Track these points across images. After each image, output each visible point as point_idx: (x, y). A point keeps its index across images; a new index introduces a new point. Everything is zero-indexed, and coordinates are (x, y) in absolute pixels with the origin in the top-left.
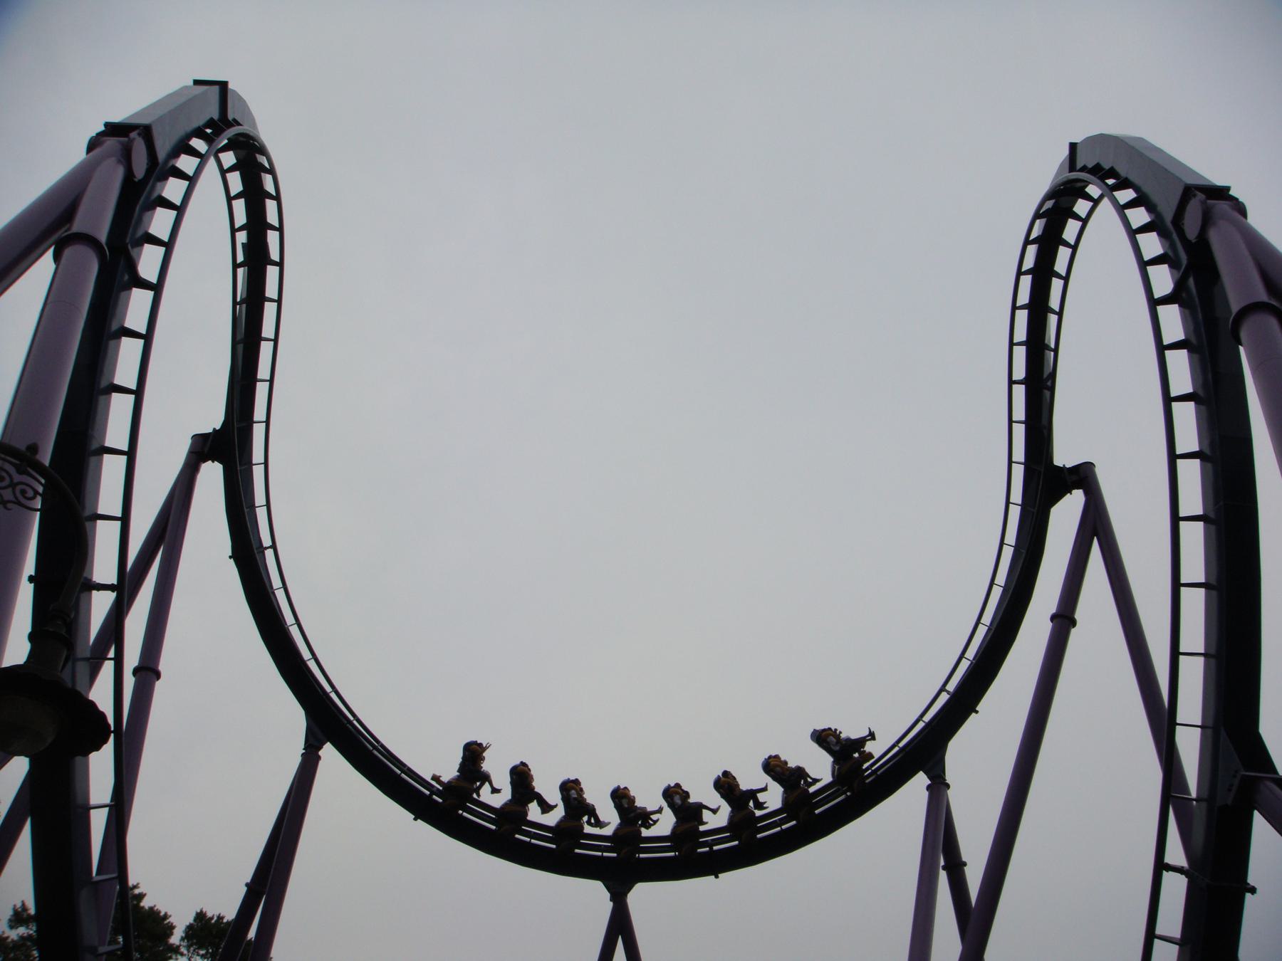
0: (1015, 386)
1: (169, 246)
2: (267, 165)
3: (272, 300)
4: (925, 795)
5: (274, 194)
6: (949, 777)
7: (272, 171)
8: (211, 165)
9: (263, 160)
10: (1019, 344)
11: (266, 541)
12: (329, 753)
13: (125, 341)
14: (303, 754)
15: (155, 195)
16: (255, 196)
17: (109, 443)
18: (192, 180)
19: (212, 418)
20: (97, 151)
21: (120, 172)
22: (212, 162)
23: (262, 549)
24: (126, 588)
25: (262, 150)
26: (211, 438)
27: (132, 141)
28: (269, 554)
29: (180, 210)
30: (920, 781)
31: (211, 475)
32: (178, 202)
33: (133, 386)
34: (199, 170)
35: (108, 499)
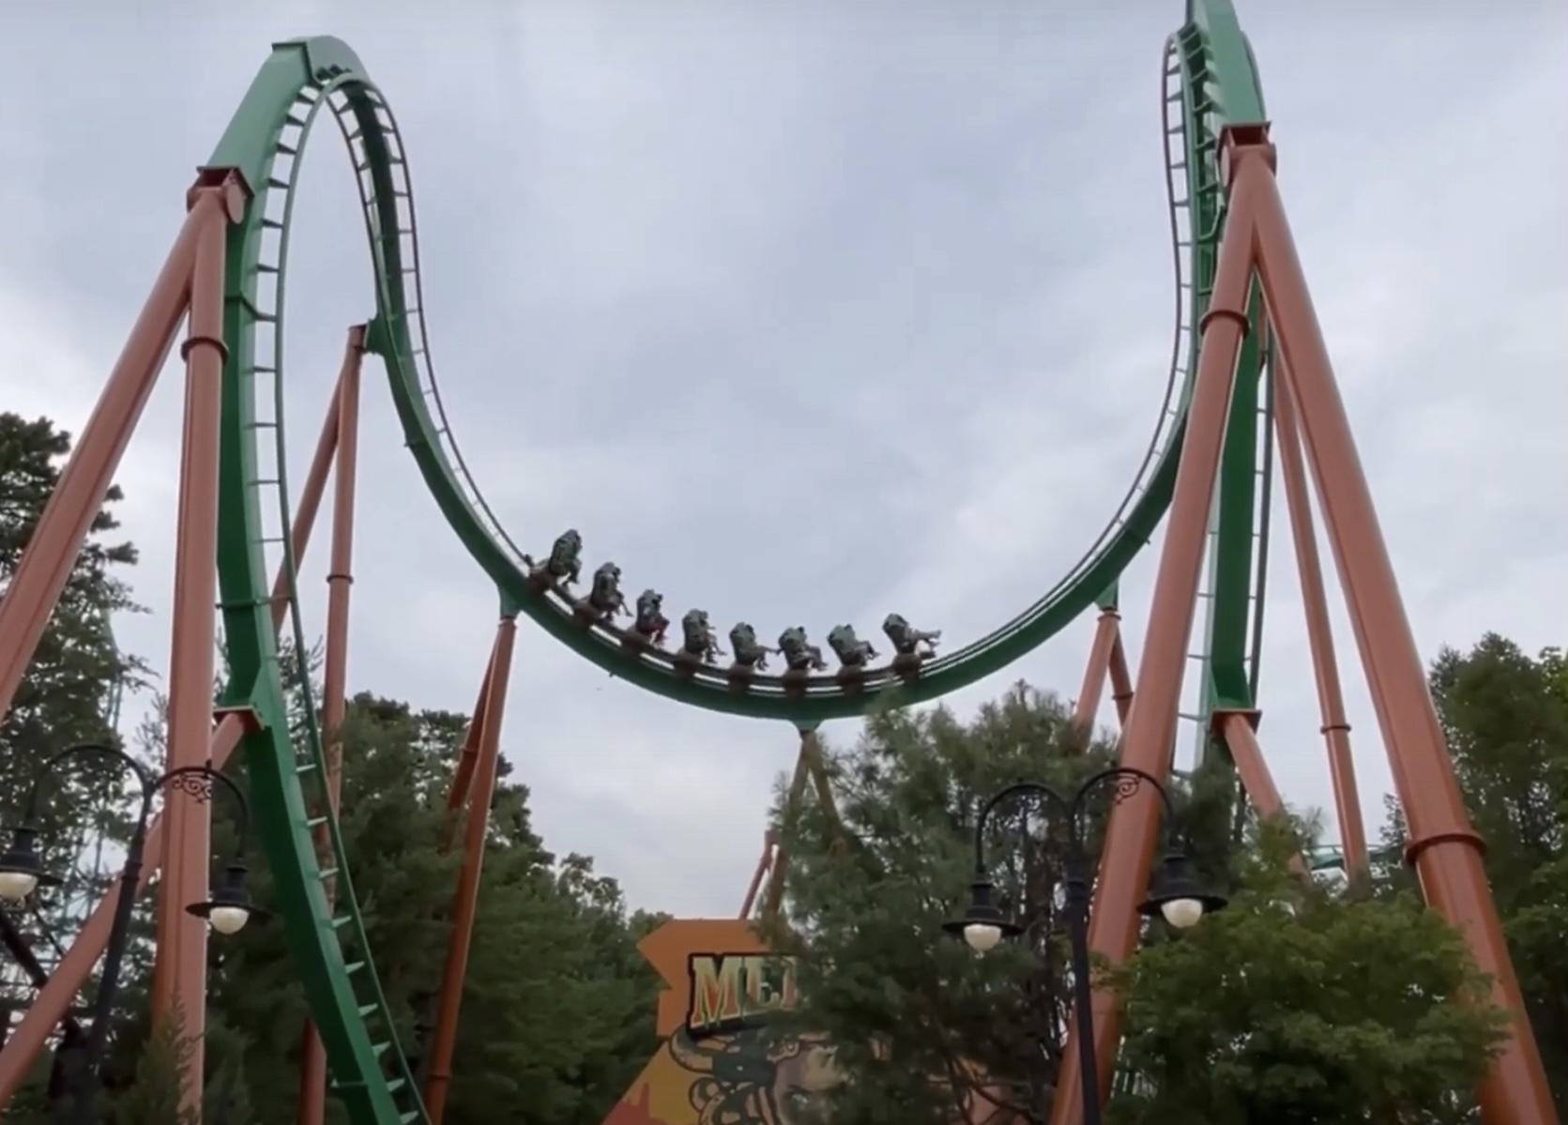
0: (1178, 210)
1: (289, 187)
2: (378, 100)
3: (405, 231)
4: (1096, 625)
5: (391, 127)
6: (1121, 611)
7: (384, 105)
8: (324, 109)
9: (370, 94)
10: (1177, 166)
11: (438, 425)
12: (524, 621)
13: (261, 276)
14: (500, 626)
15: (265, 177)
16: (373, 136)
17: (259, 419)
18: (305, 125)
19: (366, 310)
20: (198, 205)
21: (223, 223)
22: (324, 107)
23: (435, 434)
24: (296, 541)
25: (368, 86)
26: (367, 331)
27: (225, 190)
28: (444, 438)
29: (297, 154)
30: (1092, 613)
31: (373, 366)
32: (286, 180)
33: (272, 366)
34: (311, 116)
35: (265, 465)
